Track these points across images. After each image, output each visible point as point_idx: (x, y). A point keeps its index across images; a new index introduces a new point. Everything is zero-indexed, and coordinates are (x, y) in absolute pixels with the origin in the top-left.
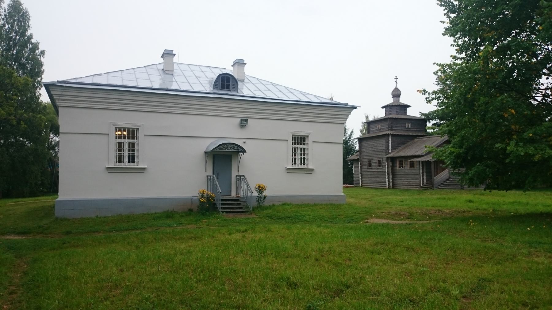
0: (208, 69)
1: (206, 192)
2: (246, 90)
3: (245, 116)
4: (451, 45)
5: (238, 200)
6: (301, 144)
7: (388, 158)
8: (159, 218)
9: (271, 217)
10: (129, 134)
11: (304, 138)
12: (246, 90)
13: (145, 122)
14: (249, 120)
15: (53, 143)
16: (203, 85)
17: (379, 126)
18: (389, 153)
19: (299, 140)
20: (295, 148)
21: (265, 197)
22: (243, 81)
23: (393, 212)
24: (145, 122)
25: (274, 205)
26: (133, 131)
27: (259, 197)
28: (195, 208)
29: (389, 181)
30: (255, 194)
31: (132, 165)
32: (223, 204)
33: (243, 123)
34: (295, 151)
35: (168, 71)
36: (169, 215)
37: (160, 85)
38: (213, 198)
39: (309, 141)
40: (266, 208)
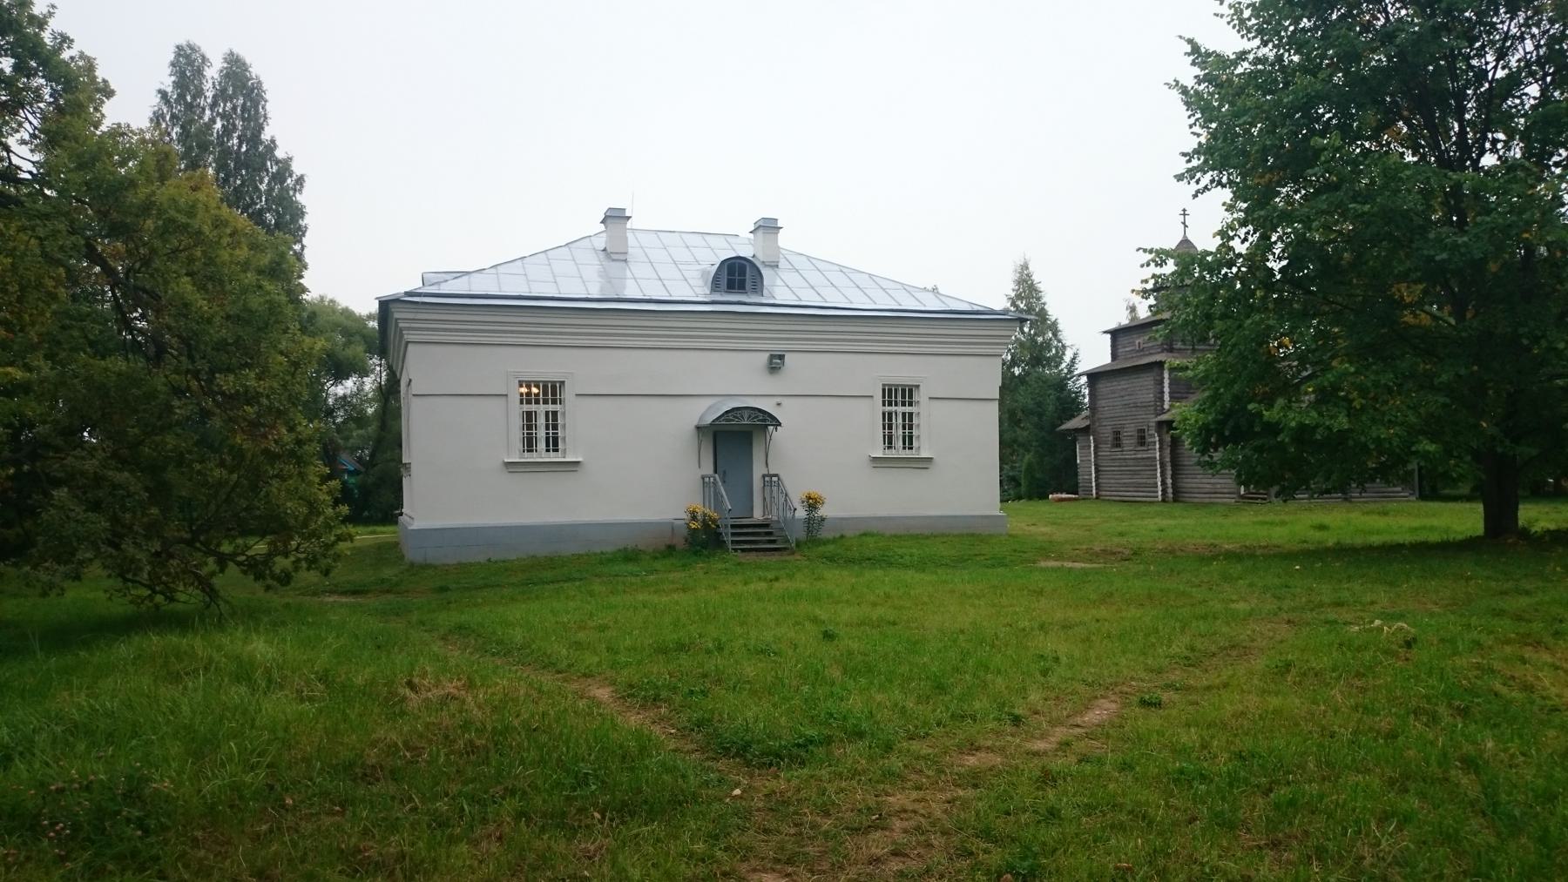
0: (697, 240)
1: (700, 510)
2: (782, 290)
3: (778, 347)
4: (1195, 196)
5: (767, 526)
6: (904, 404)
7: (1160, 424)
8: (609, 560)
9: (831, 559)
10: (545, 393)
11: (911, 391)
12: (782, 290)
13: (576, 368)
14: (788, 357)
15: (331, 401)
16: (688, 284)
17: (1140, 340)
18: (1163, 412)
19: (899, 395)
20: (890, 414)
21: (823, 519)
22: (774, 266)
23: (1097, 549)
24: (576, 368)
25: (842, 537)
26: (554, 387)
27: (809, 521)
28: (680, 543)
29: (1163, 483)
30: (801, 513)
31: (553, 457)
32: (737, 528)
33: (775, 363)
34: (890, 419)
35: (614, 255)
36: (630, 556)
37: (602, 289)
38: (714, 521)
39: (921, 397)
40: (826, 542)
